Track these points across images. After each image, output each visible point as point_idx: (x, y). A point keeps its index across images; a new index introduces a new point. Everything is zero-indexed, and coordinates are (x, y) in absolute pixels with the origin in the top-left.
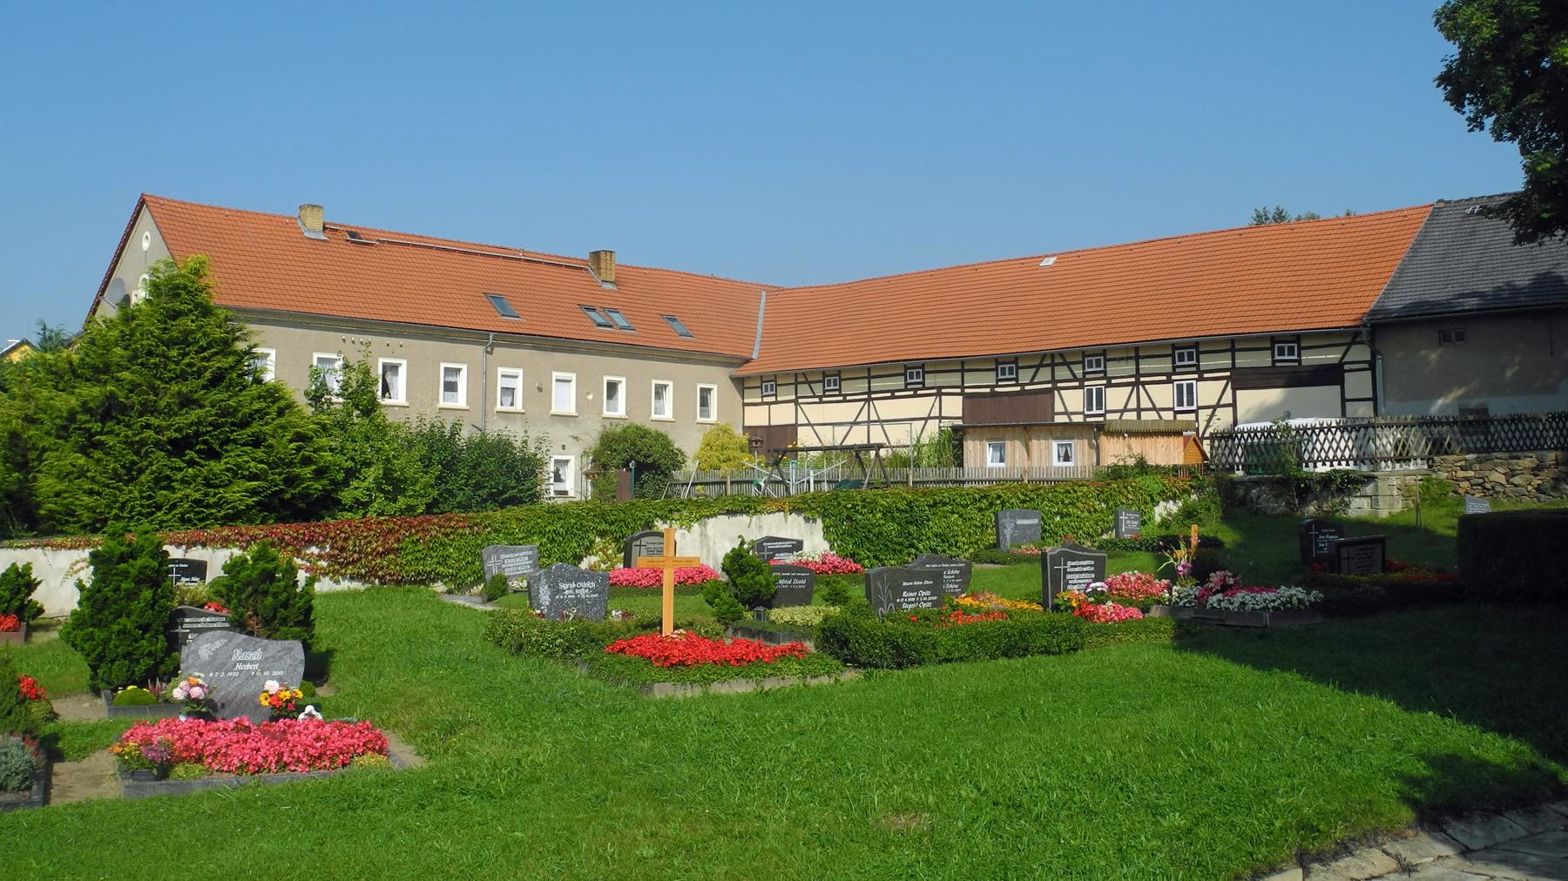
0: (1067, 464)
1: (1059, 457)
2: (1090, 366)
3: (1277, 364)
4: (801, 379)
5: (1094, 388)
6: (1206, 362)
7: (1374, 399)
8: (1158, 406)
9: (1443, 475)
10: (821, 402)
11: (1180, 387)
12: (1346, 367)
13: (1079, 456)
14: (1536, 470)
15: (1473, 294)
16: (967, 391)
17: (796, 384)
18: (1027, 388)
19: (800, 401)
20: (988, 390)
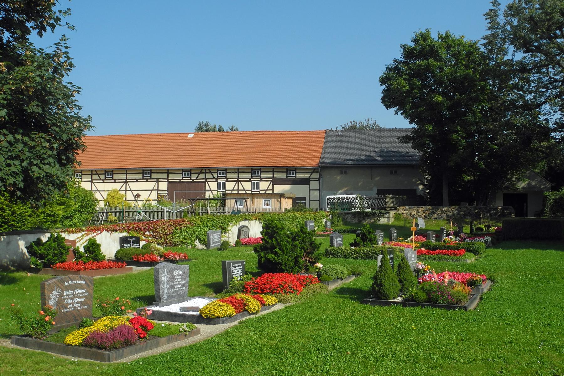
0: (268, 207)
1: (265, 204)
2: (220, 174)
3: (288, 177)
4: (94, 173)
5: (222, 182)
6: (263, 175)
7: (319, 190)
8: (245, 189)
9: (400, 212)
10: (104, 182)
11: (254, 183)
12: (311, 179)
13: (273, 204)
14: (424, 211)
15: (350, 160)
16: (169, 180)
17: (92, 174)
18: (195, 180)
19: (93, 181)
20: (179, 181)
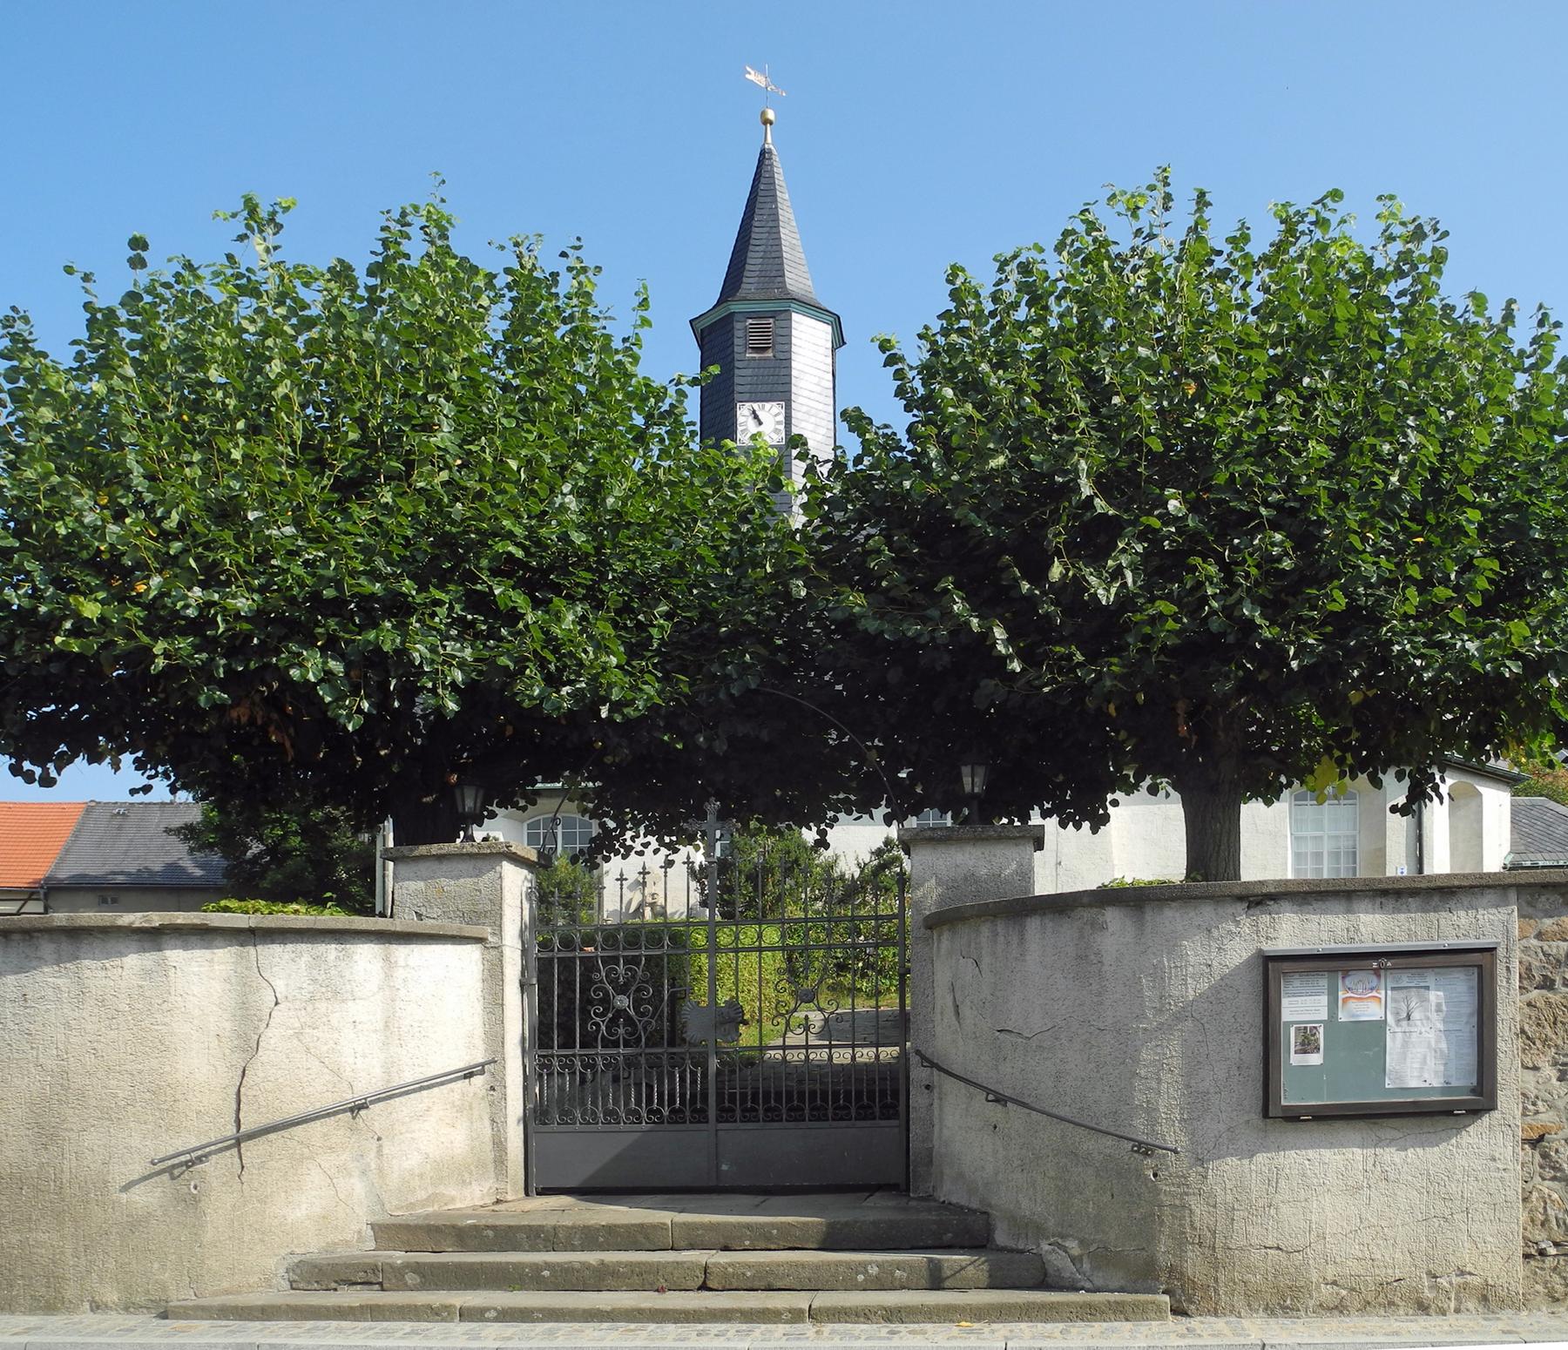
15: (122, 873)
